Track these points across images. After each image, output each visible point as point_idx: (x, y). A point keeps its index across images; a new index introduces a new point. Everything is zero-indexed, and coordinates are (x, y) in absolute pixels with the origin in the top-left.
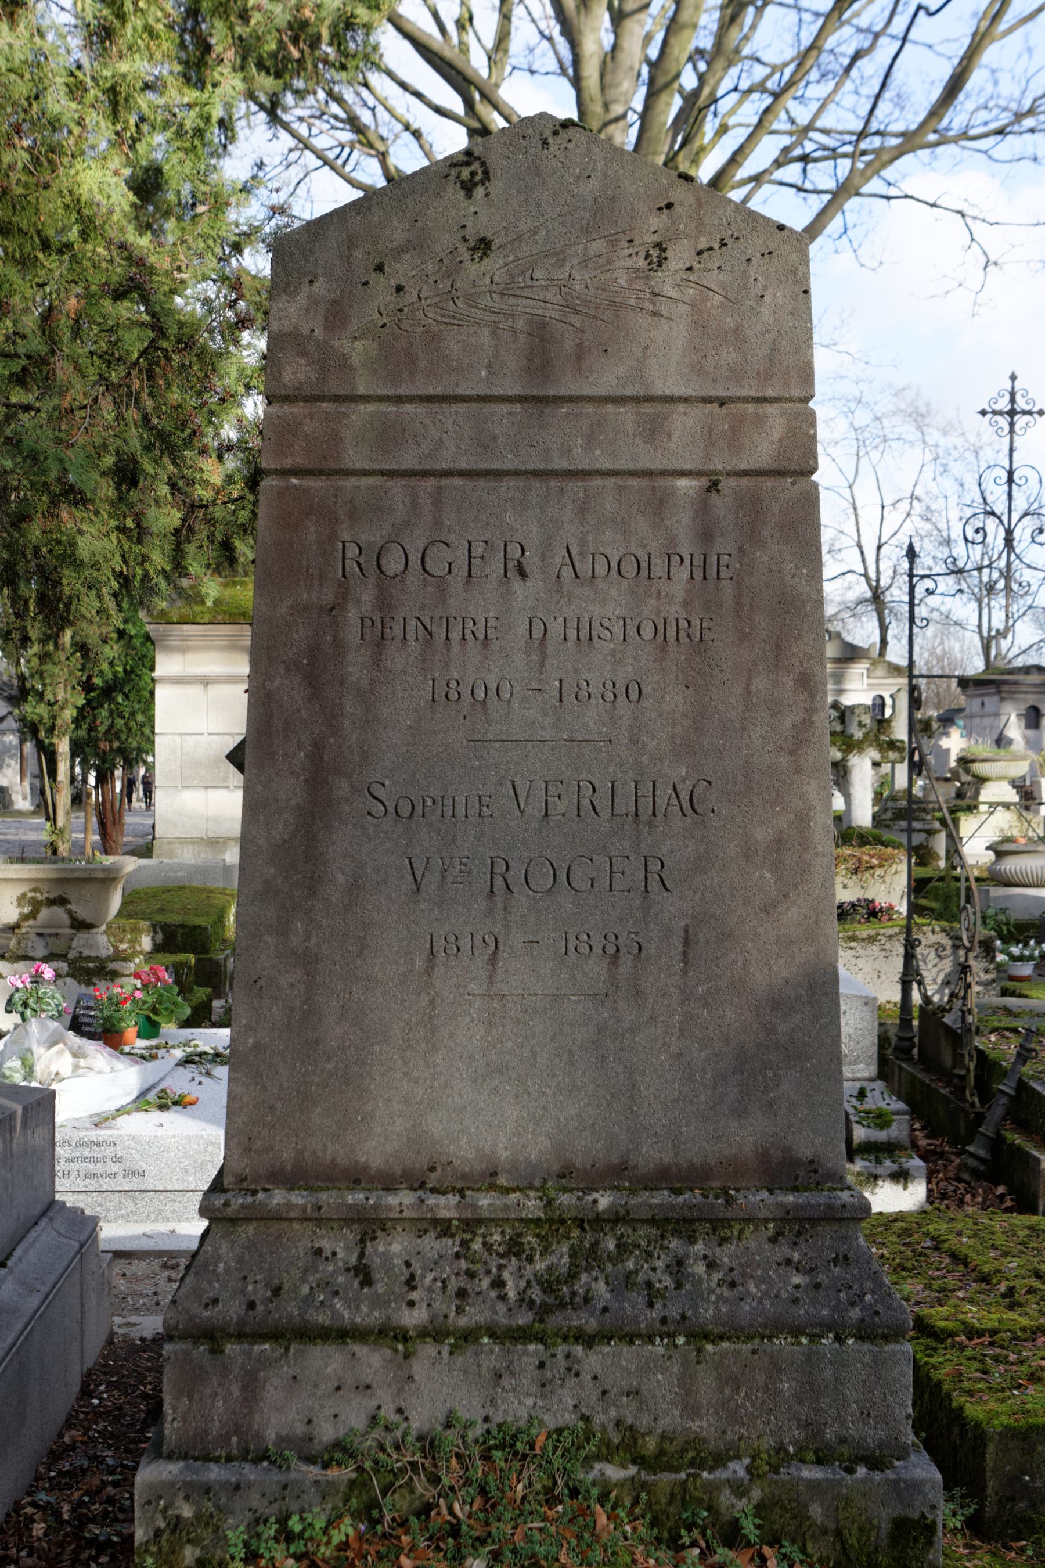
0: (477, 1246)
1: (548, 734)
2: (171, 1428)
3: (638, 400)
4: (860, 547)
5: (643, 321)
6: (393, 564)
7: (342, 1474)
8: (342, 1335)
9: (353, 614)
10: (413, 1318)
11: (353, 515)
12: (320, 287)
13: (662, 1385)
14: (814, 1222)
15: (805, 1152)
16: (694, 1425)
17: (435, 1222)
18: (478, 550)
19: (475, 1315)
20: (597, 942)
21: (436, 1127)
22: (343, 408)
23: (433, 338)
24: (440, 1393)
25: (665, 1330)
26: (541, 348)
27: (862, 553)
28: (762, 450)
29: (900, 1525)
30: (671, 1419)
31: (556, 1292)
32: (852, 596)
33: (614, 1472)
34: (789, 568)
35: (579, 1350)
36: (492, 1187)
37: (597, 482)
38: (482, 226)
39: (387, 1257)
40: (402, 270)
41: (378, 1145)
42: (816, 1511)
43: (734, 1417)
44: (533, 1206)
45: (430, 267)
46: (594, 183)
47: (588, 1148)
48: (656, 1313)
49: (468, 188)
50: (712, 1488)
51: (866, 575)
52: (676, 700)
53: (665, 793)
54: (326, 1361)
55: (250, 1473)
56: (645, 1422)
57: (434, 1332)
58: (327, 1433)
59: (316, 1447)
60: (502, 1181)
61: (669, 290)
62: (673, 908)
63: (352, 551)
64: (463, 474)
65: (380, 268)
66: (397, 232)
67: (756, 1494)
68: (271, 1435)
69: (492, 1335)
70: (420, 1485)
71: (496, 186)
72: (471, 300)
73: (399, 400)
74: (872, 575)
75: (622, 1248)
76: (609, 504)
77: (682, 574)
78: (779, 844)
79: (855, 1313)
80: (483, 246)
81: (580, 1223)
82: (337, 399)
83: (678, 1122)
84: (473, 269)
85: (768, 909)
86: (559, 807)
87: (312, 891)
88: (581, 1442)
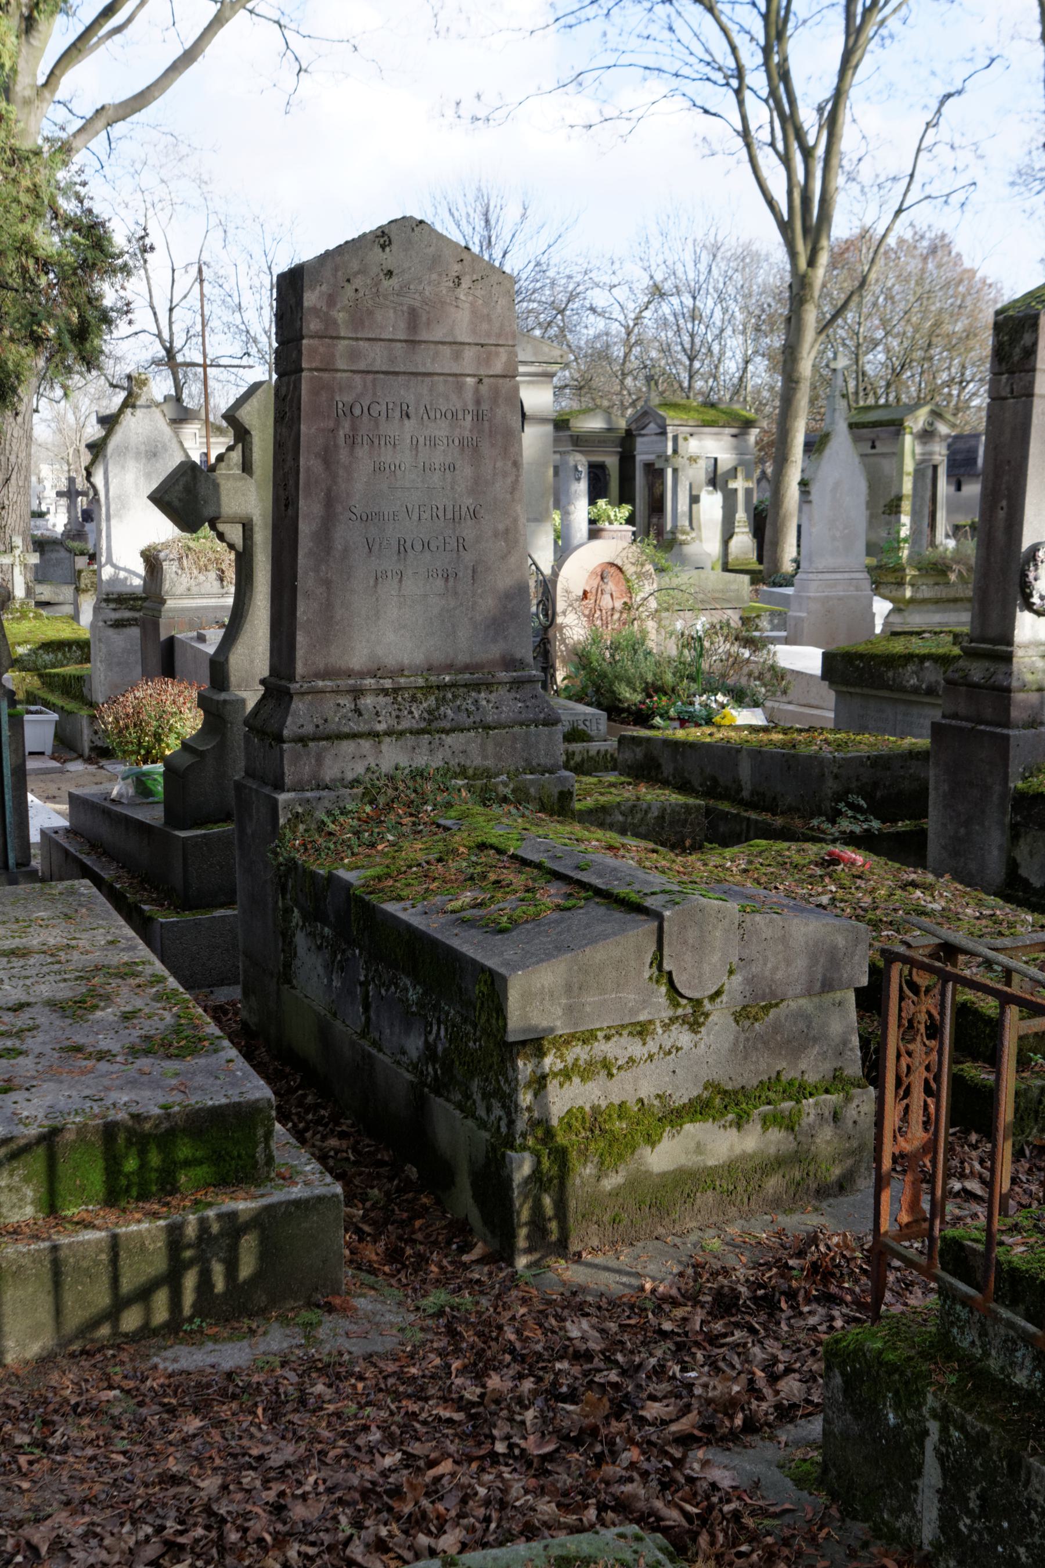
0: (399, 699)
1: (419, 485)
2: (288, 780)
3: (450, 343)
4: (153, 308)
5: (453, 310)
6: (357, 411)
7: (360, 790)
8: (354, 736)
9: (341, 433)
10: (381, 727)
11: (341, 390)
12: (324, 288)
13: (474, 748)
14: (523, 682)
15: (518, 656)
16: (486, 763)
17: (383, 690)
18: (391, 406)
19: (405, 724)
20: (440, 572)
21: (380, 651)
22: (335, 342)
23: (370, 313)
24: (392, 756)
25: (474, 727)
26: (413, 318)
27: (155, 314)
28: (498, 368)
29: (561, 793)
30: (478, 761)
31: (432, 715)
32: (146, 356)
33: (460, 782)
34: (509, 416)
35: (444, 736)
36: (402, 675)
37: (436, 378)
38: (389, 265)
39: (366, 705)
40: (358, 282)
41: (358, 658)
42: (532, 790)
43: (500, 759)
44: (421, 682)
45: (369, 281)
46: (432, 249)
47: (438, 658)
48: (472, 719)
49: (383, 247)
50: (496, 784)
51: (159, 336)
52: (468, 471)
53: (464, 510)
54: (348, 747)
55: (325, 793)
56: (468, 763)
57: (388, 733)
58: (350, 776)
59: (346, 782)
60: (406, 673)
61: (462, 297)
62: (468, 557)
63: (340, 405)
64: (383, 373)
65: (348, 281)
66: (355, 265)
67: (511, 786)
68: (328, 779)
69: (411, 733)
70: (390, 791)
71: (394, 247)
72: (385, 297)
73: (357, 339)
74: (166, 335)
75: (455, 697)
76: (441, 388)
77: (469, 418)
78: (507, 531)
79: (542, 716)
80: (390, 273)
81: (438, 687)
82: (332, 338)
83: (467, 645)
84: (386, 283)
85: (504, 558)
86: (424, 516)
87: (328, 554)
88: (447, 772)
